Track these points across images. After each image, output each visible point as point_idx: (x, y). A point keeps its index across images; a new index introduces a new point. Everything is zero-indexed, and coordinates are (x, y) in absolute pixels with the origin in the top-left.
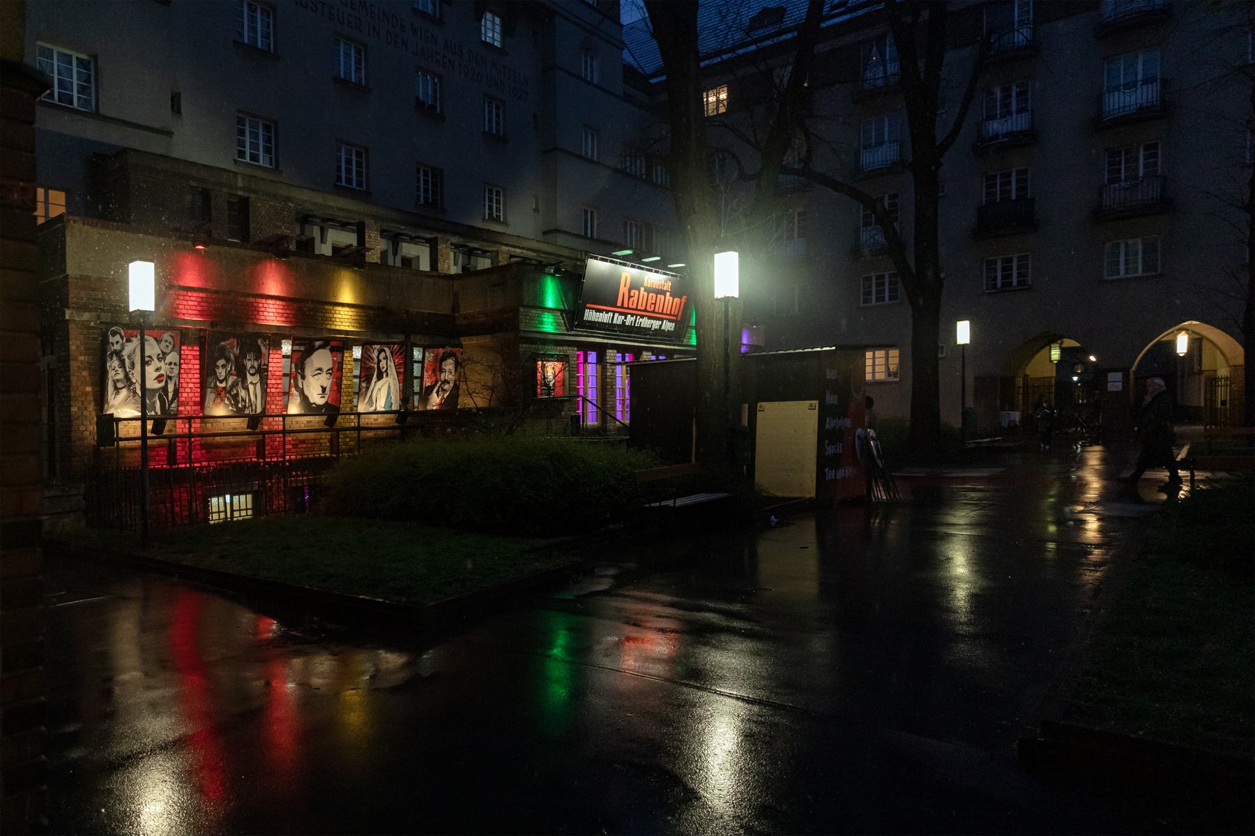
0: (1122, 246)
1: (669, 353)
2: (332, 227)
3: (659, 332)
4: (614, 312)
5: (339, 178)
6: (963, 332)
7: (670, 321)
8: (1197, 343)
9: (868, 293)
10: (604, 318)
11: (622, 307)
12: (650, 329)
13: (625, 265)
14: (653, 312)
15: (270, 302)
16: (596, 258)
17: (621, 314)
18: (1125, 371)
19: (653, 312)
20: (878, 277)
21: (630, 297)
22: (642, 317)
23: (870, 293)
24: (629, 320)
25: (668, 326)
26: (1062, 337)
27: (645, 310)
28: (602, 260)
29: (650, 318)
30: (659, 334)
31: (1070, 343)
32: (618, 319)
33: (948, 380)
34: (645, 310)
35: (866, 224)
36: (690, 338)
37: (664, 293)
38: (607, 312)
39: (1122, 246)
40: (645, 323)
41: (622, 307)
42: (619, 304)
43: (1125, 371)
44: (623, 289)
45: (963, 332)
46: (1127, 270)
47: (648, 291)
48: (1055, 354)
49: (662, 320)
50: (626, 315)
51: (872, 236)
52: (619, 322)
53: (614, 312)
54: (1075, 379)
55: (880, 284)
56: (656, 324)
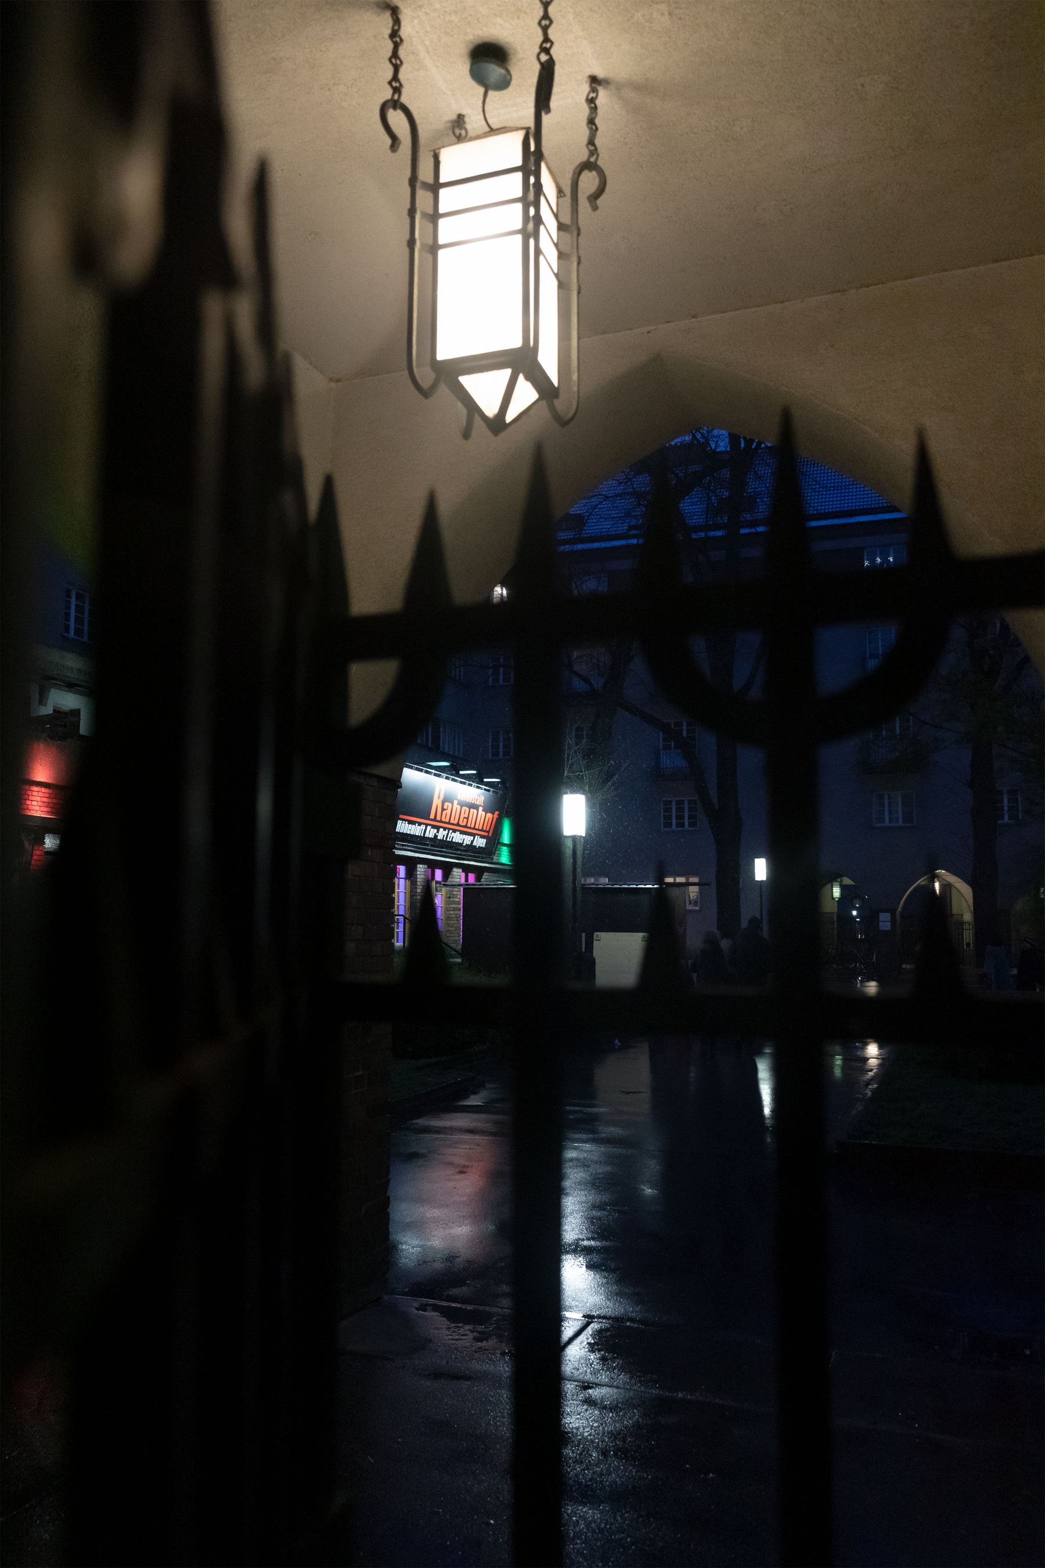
0: (886, 797)
1: (479, 872)
2: (56, 686)
3: (471, 847)
4: (427, 825)
5: (67, 629)
6: (761, 869)
7: (482, 837)
8: (946, 887)
9: (668, 818)
10: (416, 830)
11: (435, 820)
12: (461, 844)
13: (464, 783)
14: (466, 827)
15: (35, 789)
16: (412, 768)
17: (434, 827)
18: (893, 911)
19: (466, 827)
20: (679, 803)
21: (443, 810)
22: (454, 831)
23: (670, 817)
24: (442, 834)
25: (480, 842)
26: (841, 876)
27: (458, 825)
28: (417, 769)
29: (462, 833)
30: (471, 851)
31: (847, 881)
32: (431, 833)
33: (750, 909)
34: (449, 823)
35: (667, 748)
36: (499, 855)
37: (475, 806)
38: (420, 824)
39: (886, 797)
40: (457, 837)
41: (435, 820)
42: (432, 816)
43: (893, 911)
44: (436, 802)
45: (761, 869)
46: (890, 820)
47: (462, 804)
48: (837, 892)
49: (474, 835)
50: (438, 828)
51: (673, 761)
52: (431, 836)
53: (427, 825)
54: (854, 913)
55: (680, 810)
56: (467, 840)
